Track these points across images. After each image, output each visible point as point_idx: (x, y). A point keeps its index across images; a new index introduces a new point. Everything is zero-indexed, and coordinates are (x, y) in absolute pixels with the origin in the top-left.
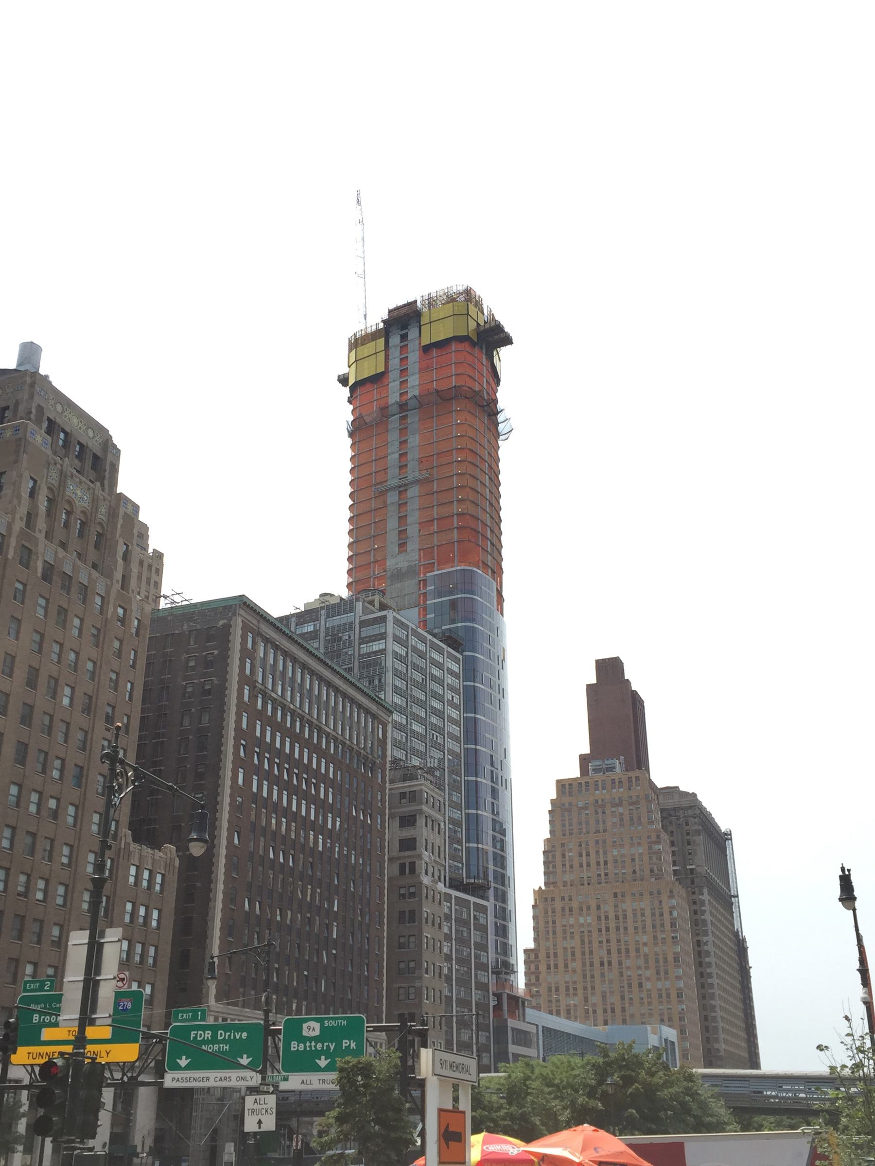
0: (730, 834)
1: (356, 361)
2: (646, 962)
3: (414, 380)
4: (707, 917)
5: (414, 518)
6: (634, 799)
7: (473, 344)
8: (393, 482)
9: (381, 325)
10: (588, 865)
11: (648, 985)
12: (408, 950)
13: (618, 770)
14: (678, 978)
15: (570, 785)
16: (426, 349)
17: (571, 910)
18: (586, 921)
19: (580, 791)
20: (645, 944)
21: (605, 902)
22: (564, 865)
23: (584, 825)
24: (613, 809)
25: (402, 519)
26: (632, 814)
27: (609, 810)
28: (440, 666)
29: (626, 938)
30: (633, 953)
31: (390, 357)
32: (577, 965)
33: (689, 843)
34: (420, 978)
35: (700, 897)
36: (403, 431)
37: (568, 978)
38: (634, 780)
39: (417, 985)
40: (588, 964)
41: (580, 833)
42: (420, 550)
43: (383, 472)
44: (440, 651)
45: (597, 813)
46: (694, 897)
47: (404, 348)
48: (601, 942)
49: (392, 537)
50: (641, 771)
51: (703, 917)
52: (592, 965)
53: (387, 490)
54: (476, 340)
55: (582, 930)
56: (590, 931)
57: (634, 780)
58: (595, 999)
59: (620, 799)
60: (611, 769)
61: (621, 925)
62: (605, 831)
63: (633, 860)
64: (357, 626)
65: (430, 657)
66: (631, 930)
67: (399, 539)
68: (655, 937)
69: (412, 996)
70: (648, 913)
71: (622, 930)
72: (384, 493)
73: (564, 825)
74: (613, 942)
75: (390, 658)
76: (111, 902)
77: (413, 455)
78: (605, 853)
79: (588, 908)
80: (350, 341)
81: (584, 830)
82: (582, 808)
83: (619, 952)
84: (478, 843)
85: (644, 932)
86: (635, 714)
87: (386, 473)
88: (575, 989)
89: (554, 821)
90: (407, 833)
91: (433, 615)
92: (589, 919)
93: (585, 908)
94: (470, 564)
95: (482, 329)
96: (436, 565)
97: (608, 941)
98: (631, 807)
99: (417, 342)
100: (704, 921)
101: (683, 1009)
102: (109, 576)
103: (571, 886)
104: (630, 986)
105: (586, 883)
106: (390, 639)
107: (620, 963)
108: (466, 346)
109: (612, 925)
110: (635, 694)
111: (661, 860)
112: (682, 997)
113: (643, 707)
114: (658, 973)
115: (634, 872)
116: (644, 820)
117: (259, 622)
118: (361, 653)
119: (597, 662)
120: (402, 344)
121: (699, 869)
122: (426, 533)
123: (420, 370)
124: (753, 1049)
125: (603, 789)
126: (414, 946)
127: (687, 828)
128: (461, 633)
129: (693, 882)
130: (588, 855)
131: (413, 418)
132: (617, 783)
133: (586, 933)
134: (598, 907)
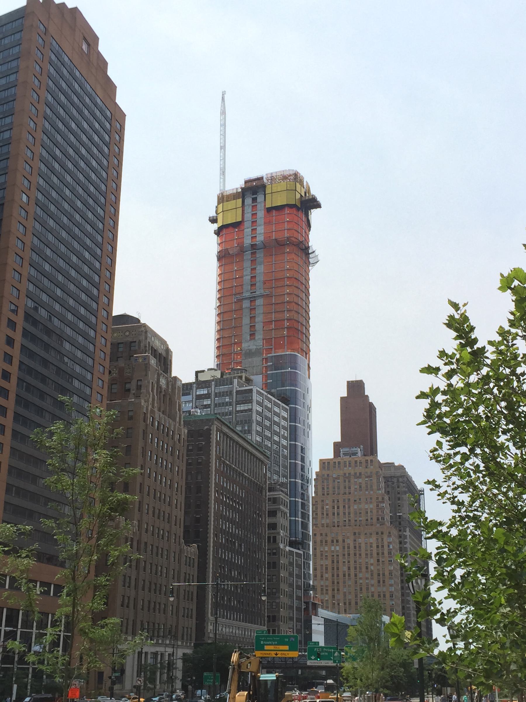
0: (423, 491)
1: (223, 211)
2: (372, 575)
3: (260, 230)
4: (408, 546)
5: (260, 319)
6: (369, 474)
7: (298, 209)
8: (247, 294)
9: (240, 190)
10: (338, 514)
11: (373, 589)
12: (272, 583)
13: (359, 454)
14: (391, 585)
15: (328, 463)
16: (269, 210)
17: (326, 542)
18: (335, 548)
19: (335, 467)
20: (372, 564)
21: (348, 538)
22: (323, 514)
23: (336, 490)
24: (356, 480)
25: (252, 318)
26: (367, 483)
27: (353, 480)
28: (278, 415)
29: (360, 561)
30: (364, 569)
31: (245, 211)
32: (328, 575)
33: (399, 499)
34: (279, 597)
35: (404, 533)
36: (253, 262)
37: (322, 583)
38: (369, 461)
39: (277, 601)
40: (335, 575)
41: (334, 494)
42: (263, 339)
43: (240, 287)
44: (278, 406)
45: (345, 481)
46: (400, 533)
47: (254, 207)
48: (344, 562)
49: (246, 330)
50: (374, 456)
51: (405, 546)
52: (338, 576)
53: (242, 299)
54: (300, 207)
55: (333, 554)
56: (338, 556)
57: (369, 461)
58: (340, 596)
59: (360, 474)
60: (355, 454)
61: (358, 552)
62: (350, 493)
63: (367, 513)
64: (235, 394)
65: (274, 410)
66: (363, 555)
67: (250, 331)
68: (378, 561)
69: (274, 607)
70: (374, 545)
71: (358, 555)
72: (240, 301)
73: (323, 489)
74: (352, 562)
75: (254, 415)
76: (168, 571)
77: (260, 278)
78: (349, 507)
79: (337, 541)
80: (218, 197)
81: (336, 492)
82: (336, 478)
83: (355, 568)
84: (296, 517)
85: (372, 557)
86: (371, 418)
87: (242, 288)
88: (327, 590)
89: (317, 486)
90: (272, 520)
91: (271, 381)
92: (338, 548)
93: (335, 541)
94: (293, 350)
95: (303, 199)
96: (273, 349)
97: (349, 562)
98: (367, 479)
99: (263, 205)
100: (406, 548)
101: (393, 604)
102: (174, 420)
103: (327, 527)
104: (361, 589)
105: (336, 526)
106: (254, 403)
107: (356, 575)
108: (294, 211)
109: (352, 552)
110: (371, 406)
111: (384, 513)
112: (393, 597)
113: (375, 412)
114: (379, 582)
115: (367, 520)
116: (375, 487)
117: (222, 425)
118: (237, 410)
119: (348, 382)
120: (253, 204)
121: (404, 516)
122: (268, 329)
123: (265, 223)
124: (430, 626)
125: (349, 467)
126: (275, 581)
127: (398, 489)
128: (288, 394)
129: (400, 524)
130: (338, 508)
131: (260, 255)
132: (358, 463)
133: (335, 556)
134: (344, 541)
